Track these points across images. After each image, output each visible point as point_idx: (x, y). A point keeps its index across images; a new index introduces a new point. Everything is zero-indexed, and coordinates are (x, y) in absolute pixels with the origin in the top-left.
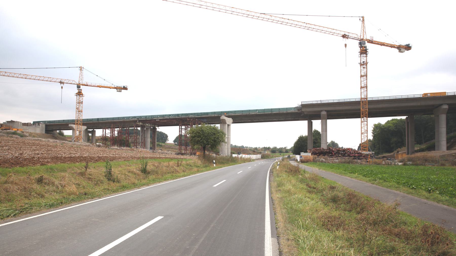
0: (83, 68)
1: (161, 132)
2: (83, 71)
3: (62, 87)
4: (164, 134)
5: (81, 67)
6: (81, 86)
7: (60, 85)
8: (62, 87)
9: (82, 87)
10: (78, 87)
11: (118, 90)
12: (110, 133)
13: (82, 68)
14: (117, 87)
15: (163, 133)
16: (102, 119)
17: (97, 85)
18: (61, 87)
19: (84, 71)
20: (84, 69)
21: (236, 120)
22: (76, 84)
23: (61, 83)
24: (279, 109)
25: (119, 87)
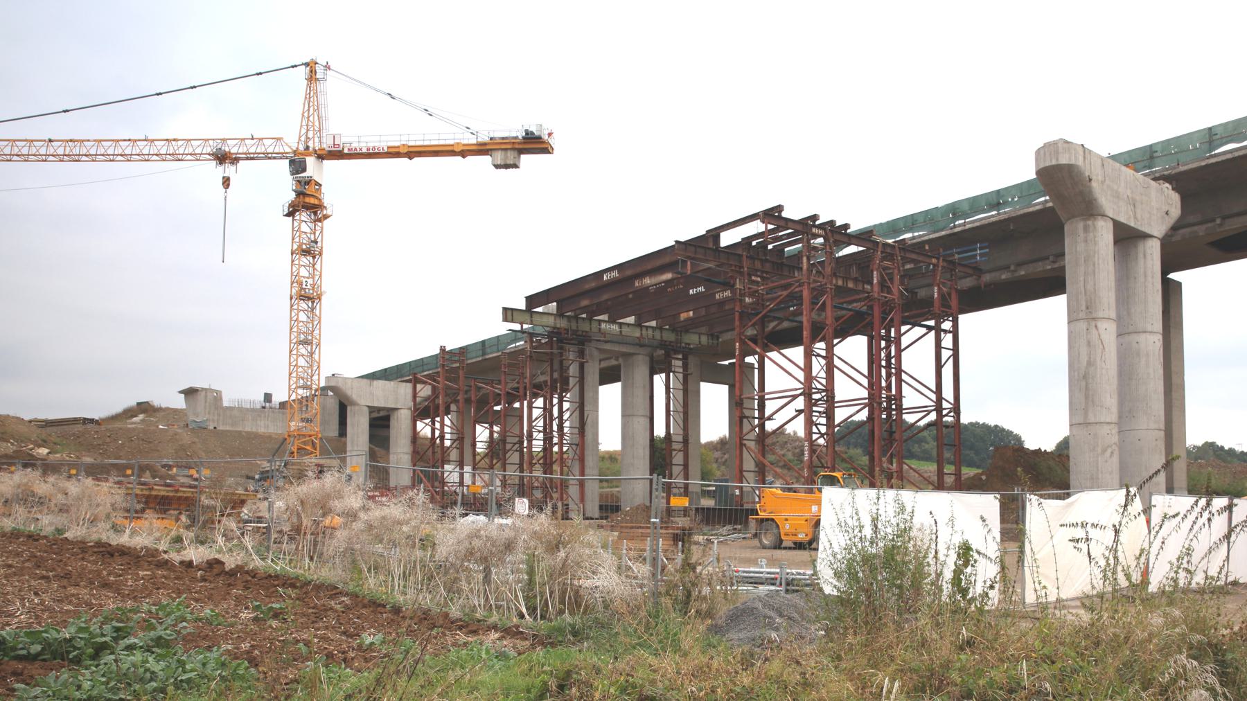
0: (327, 67)
1: (996, 426)
2: (320, 86)
3: (226, 182)
4: (1009, 433)
5: (311, 66)
6: (311, 161)
7: (216, 172)
8: (226, 182)
9: (312, 168)
10: (297, 166)
11: (499, 157)
12: (800, 403)
13: (319, 69)
14: (491, 139)
15: (1003, 430)
16: (408, 365)
17: (383, 145)
18: (221, 181)
19: (331, 87)
20: (329, 72)
21: (1224, 218)
22: (282, 156)
23: (222, 158)
24: (410, 365)
25: (503, 138)
